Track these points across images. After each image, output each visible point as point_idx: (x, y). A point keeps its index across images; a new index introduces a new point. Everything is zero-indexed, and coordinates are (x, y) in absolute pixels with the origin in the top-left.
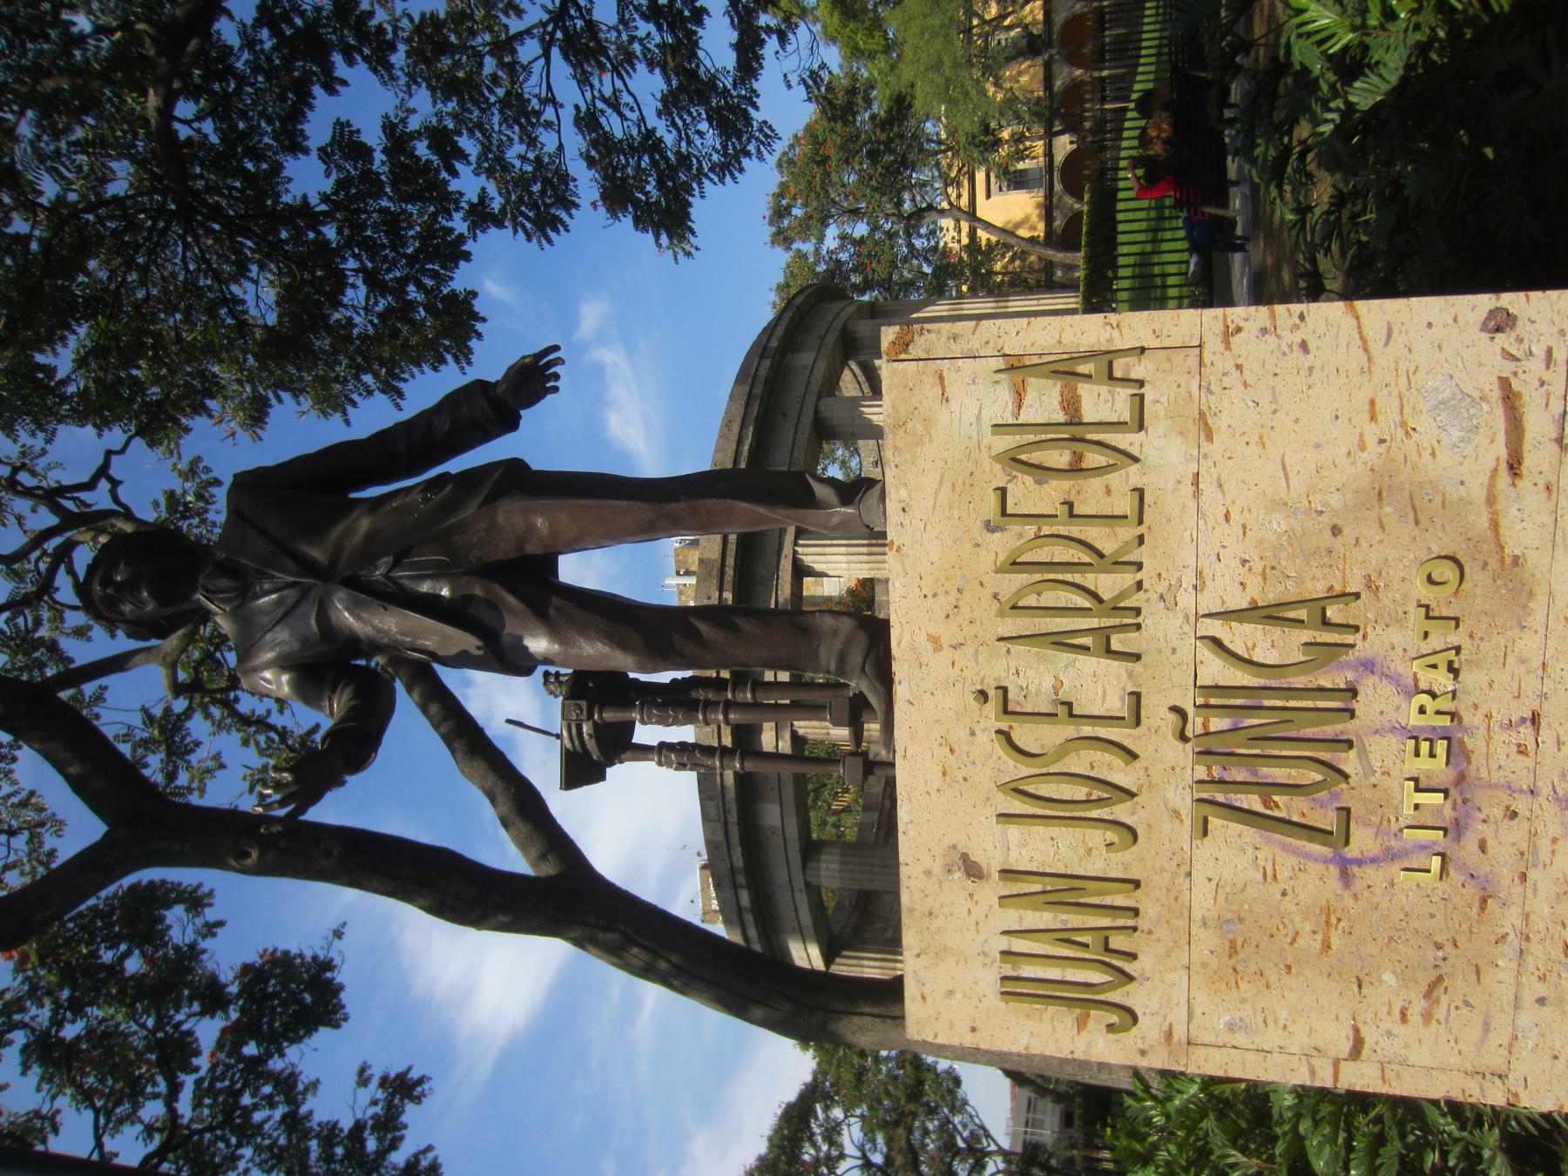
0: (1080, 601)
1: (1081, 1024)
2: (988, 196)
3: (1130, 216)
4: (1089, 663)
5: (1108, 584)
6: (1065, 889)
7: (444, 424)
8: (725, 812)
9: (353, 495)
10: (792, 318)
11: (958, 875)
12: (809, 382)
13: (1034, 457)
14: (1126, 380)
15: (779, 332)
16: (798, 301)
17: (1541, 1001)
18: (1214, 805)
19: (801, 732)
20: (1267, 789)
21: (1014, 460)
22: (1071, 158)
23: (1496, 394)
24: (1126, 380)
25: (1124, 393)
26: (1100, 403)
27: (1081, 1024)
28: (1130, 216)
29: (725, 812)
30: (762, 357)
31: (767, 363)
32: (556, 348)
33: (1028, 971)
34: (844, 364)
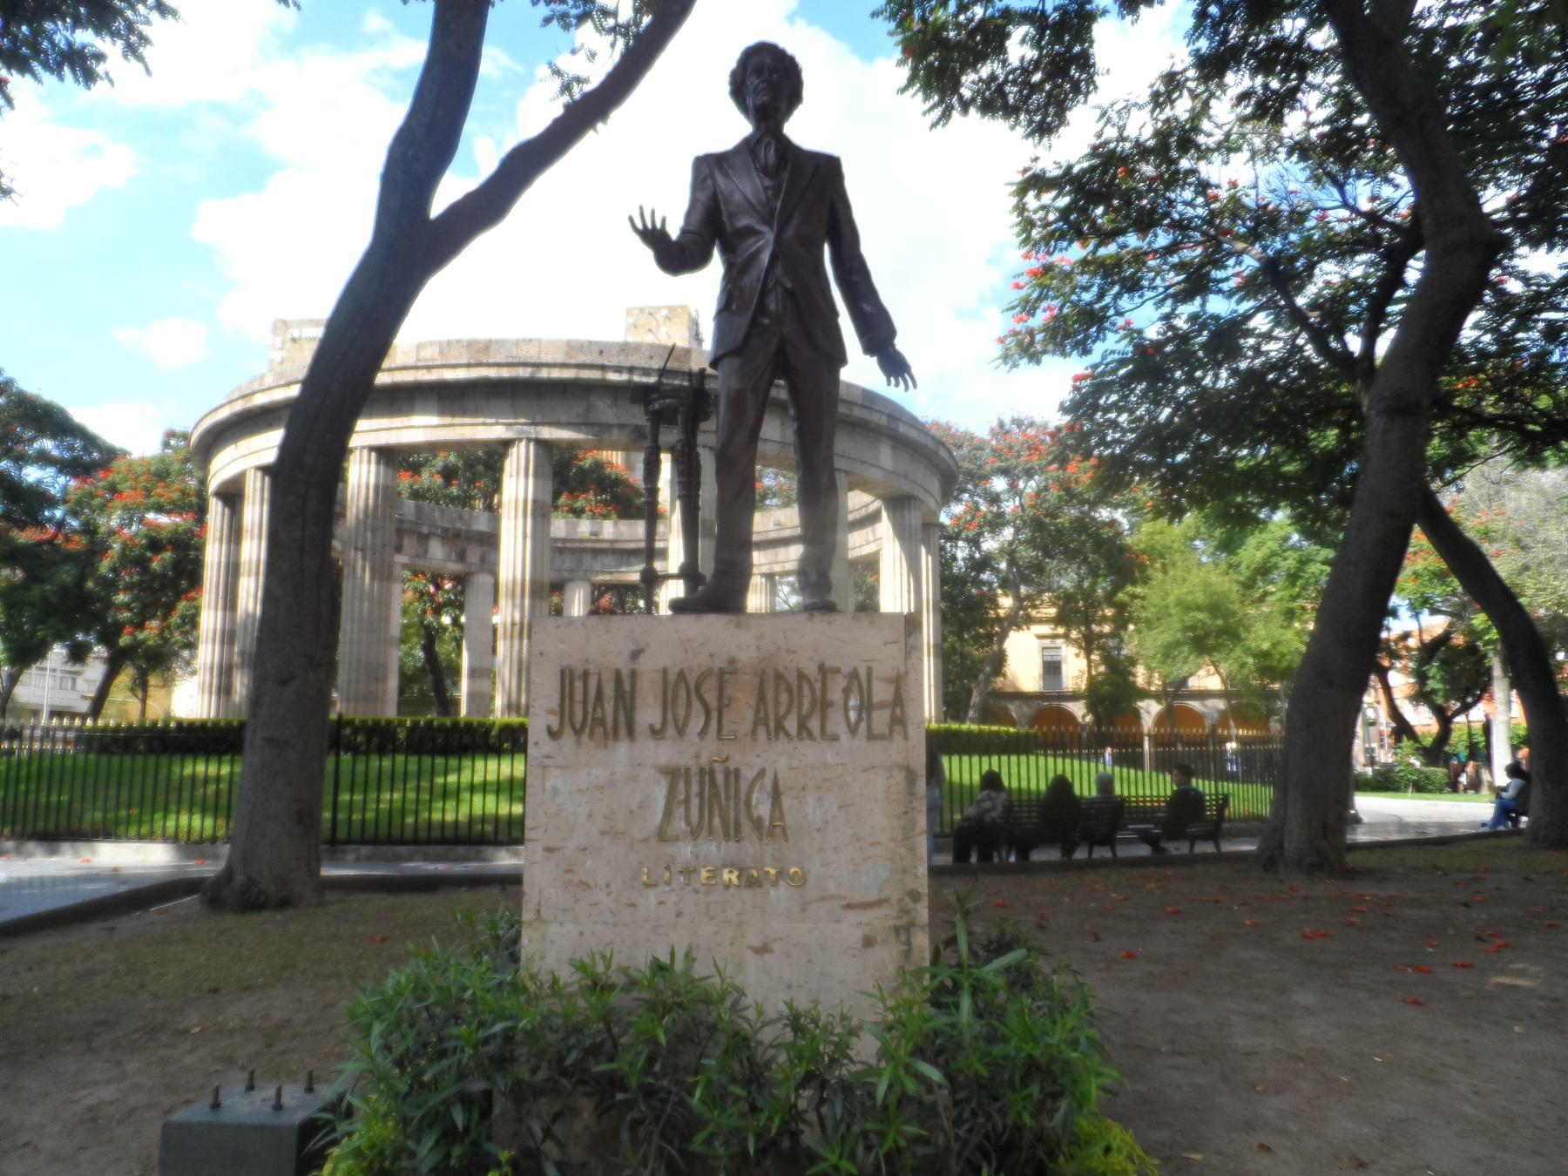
0: (783, 709)
1: (551, 712)
2: (1041, 637)
3: (1014, 770)
4: (750, 715)
5: (791, 724)
6: (626, 699)
7: (867, 308)
8: (428, 368)
9: (826, 249)
10: (926, 446)
11: (633, 647)
12: (862, 463)
13: (855, 688)
14: (891, 731)
15: (913, 434)
16: (942, 452)
17: (581, 934)
18: (673, 774)
19: (513, 451)
20: (687, 802)
21: (854, 675)
22: (1070, 717)
23: (882, 896)
24: (891, 731)
25: (885, 730)
26: (881, 719)
27: (551, 712)
28: (1014, 770)
29: (428, 368)
30: (890, 416)
31: (884, 421)
32: (915, 386)
33: (578, 684)
34: (878, 497)
